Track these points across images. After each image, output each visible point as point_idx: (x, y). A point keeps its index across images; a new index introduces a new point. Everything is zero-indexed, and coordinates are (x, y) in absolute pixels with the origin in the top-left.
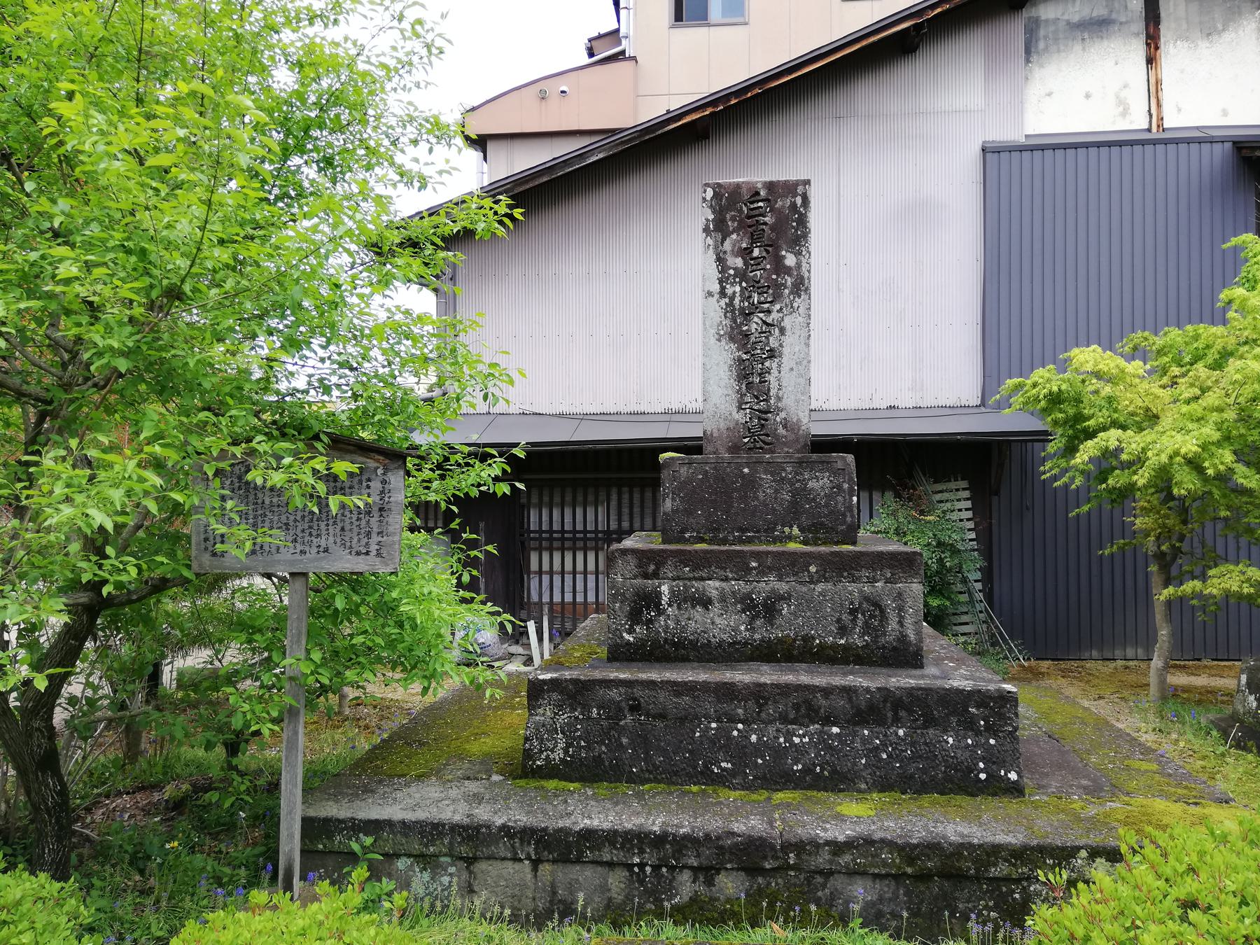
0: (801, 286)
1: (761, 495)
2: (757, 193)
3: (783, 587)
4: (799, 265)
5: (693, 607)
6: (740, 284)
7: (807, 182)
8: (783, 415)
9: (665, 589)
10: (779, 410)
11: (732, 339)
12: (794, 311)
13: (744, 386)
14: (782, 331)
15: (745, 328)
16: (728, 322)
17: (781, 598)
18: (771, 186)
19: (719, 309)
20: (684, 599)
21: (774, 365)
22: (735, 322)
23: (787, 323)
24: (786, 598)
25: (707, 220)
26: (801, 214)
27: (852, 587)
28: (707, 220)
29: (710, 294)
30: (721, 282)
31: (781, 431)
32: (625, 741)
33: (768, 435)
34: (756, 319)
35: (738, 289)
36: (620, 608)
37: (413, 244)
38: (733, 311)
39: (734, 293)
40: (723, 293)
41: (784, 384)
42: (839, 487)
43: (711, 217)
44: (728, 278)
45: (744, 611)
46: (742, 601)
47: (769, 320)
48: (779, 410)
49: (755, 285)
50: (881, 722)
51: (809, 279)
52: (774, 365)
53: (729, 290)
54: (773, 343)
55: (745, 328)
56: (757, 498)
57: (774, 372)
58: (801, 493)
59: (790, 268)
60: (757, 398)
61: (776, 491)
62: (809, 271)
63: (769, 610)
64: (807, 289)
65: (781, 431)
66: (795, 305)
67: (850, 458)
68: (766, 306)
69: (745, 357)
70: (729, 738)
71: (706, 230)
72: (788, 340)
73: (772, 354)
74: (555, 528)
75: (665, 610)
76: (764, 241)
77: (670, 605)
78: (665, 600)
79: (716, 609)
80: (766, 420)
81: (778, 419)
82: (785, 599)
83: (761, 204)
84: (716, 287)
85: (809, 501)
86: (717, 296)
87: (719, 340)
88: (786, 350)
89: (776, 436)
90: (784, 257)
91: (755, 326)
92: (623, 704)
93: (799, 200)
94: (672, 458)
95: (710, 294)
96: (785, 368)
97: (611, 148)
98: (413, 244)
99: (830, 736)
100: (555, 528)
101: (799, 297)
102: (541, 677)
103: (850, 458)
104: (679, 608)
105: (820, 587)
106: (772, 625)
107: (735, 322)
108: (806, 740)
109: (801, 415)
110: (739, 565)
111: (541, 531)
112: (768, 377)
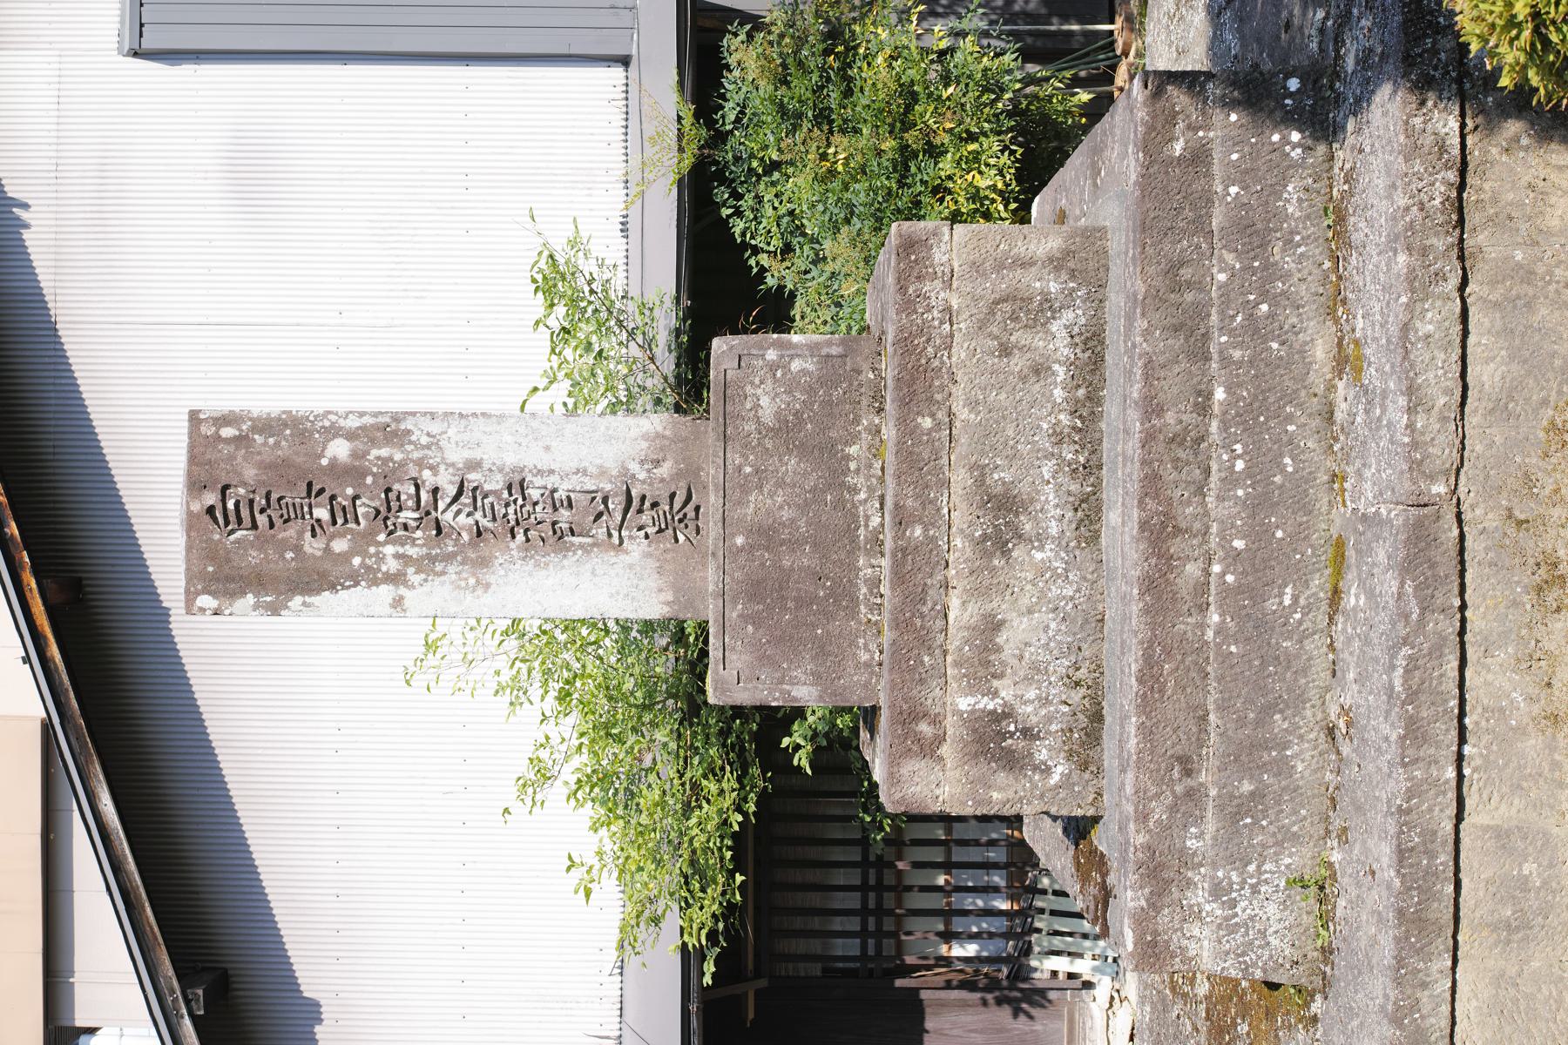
0: (390, 430)
1: (786, 514)
2: (210, 510)
3: (960, 479)
4: (351, 436)
5: (999, 650)
6: (379, 544)
7: (194, 417)
8: (634, 467)
9: (964, 703)
10: (624, 471)
11: (484, 562)
12: (434, 443)
13: (576, 540)
14: (474, 465)
15: (465, 536)
16: (452, 569)
17: (980, 482)
18: (196, 486)
19: (427, 587)
20: (984, 663)
21: (539, 481)
22: (453, 556)
23: (457, 456)
24: (980, 474)
25: (256, 607)
26: (254, 429)
27: (959, 353)
28: (256, 607)
29: (398, 603)
30: (375, 582)
31: (665, 470)
32: (1247, 787)
33: (672, 496)
34: (449, 516)
35: (389, 550)
36: (1000, 789)
37: (1327, 952)
38: (433, 559)
39: (397, 556)
40: (396, 579)
41: (574, 465)
42: (773, 367)
43: (250, 598)
44: (369, 569)
45: (1006, 553)
46: (987, 555)
47: (452, 490)
48: (624, 471)
49: (384, 516)
50: (1200, 311)
51: (376, 415)
52: (539, 481)
53: (392, 565)
54: (495, 483)
55: (465, 536)
56: (793, 521)
57: (551, 482)
58: (786, 430)
59: (355, 455)
60: (600, 515)
61: (780, 484)
62: (362, 414)
63: (1004, 511)
64: (397, 418)
65: (665, 470)
66: (424, 440)
67: (718, 344)
68: (424, 496)
69: (520, 537)
70: (1238, 589)
71: (274, 610)
72: (488, 455)
73: (517, 486)
74: (857, 905)
75: (1005, 705)
76: (300, 504)
77: (996, 694)
78: (989, 704)
79: (1001, 606)
80: (643, 498)
81: (642, 476)
82: (983, 475)
83: (231, 505)
84: (385, 592)
85: (800, 421)
86: (402, 591)
87: (487, 586)
88: (511, 459)
89: (678, 475)
90: (334, 461)
91: (462, 517)
92: (1179, 789)
93: (227, 432)
94: (715, 681)
95: (398, 603)
96: (544, 461)
97: (84, 746)
98: (1327, 952)
99: (1227, 405)
100: (857, 905)
101: (408, 432)
102: (1130, 947)
103: (718, 344)
104: (1001, 676)
105: (963, 413)
106: (1032, 501)
107: (453, 556)
108: (1238, 447)
109: (634, 433)
110: (916, 571)
111: (863, 934)
112: (561, 494)
